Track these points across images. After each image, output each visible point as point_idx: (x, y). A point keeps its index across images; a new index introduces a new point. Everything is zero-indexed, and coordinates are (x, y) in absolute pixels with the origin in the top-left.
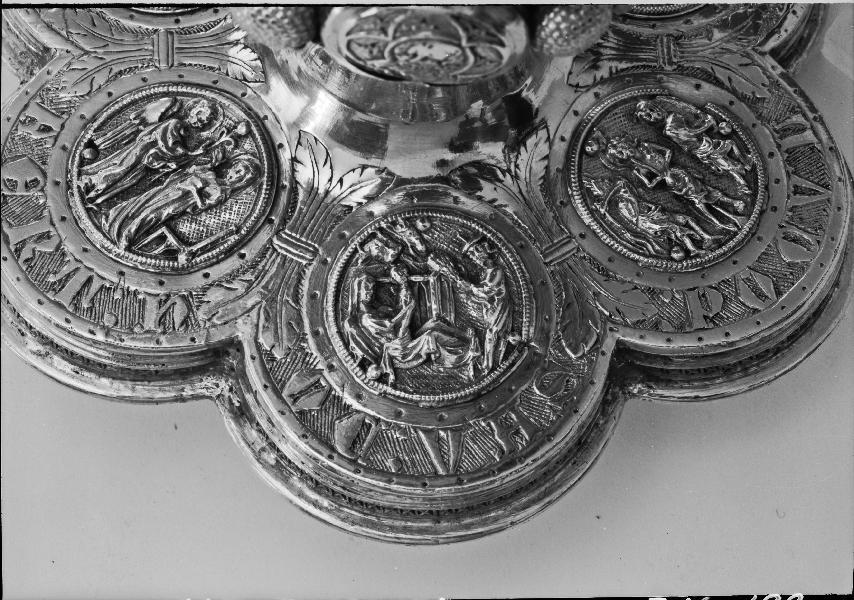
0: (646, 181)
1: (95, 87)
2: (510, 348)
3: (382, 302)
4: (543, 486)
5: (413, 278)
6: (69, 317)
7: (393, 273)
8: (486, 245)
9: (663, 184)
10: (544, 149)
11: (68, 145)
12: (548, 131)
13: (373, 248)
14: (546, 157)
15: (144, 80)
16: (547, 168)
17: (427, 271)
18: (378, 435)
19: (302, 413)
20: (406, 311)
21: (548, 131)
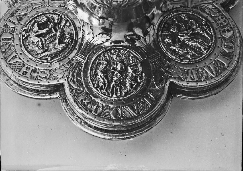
0: (112, 68)
1: (33, 8)
2: (47, 59)
3: (41, 26)
4: (148, 124)
5: (52, 29)
6: (7, 65)
7: (51, 24)
8: (71, 40)
9: (113, 73)
10: (104, 40)
11: (18, 33)
12: (110, 39)
13: (56, 17)
14: (104, 42)
15: (37, 11)
16: (101, 44)
17: (56, 31)
18: (10, 44)
19: (7, 24)
20: (44, 31)
21: (110, 39)
